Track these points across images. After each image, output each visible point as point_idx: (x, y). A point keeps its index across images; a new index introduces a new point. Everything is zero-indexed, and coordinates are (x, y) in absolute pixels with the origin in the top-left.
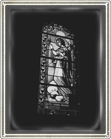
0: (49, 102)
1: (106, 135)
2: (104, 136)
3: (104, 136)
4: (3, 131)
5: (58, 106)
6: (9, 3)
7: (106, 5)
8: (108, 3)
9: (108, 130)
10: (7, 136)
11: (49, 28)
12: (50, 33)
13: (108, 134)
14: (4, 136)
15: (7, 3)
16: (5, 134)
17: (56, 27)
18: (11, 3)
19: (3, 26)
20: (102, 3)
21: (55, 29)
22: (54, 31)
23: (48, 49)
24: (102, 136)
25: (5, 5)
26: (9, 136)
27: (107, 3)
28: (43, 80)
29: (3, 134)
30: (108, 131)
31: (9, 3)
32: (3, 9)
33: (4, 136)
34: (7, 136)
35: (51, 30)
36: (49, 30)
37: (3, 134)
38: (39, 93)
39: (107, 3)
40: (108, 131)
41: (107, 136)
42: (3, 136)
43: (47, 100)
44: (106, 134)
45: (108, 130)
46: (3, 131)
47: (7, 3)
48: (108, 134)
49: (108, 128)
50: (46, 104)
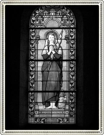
0: (40, 110)
1: (100, 131)
2: (98, 132)
3: (98, 132)
4: (3, 127)
5: (60, 80)
6: (9, 3)
7: (99, 5)
8: (101, 3)
9: (101, 126)
10: (6, 132)
11: (37, 20)
12: (39, 26)
13: (101, 131)
14: (4, 132)
15: (6, 3)
16: (5, 131)
17: (46, 17)
18: (11, 3)
19: (3, 25)
20: (95, 3)
21: (45, 19)
22: (43, 22)
23: (37, 49)
24: (95, 132)
25: (5, 5)
26: (9, 132)
27: (100, 3)
28: (32, 87)
29: (3, 131)
30: (101, 128)
31: (9, 3)
32: (3, 8)
33: (4, 132)
34: (6, 132)
35: (40, 23)
36: (37, 22)
37: (3, 131)
38: (29, 101)
39: (100, 3)
40: (101, 128)
41: (101, 132)
42: (3, 132)
43: (37, 108)
44: (99, 130)
45: (101, 126)
46: (3, 127)
47: (6, 3)
48: (101, 131)
49: (101, 125)
50: (36, 112)
